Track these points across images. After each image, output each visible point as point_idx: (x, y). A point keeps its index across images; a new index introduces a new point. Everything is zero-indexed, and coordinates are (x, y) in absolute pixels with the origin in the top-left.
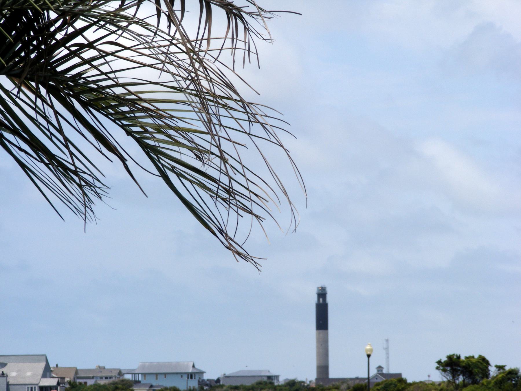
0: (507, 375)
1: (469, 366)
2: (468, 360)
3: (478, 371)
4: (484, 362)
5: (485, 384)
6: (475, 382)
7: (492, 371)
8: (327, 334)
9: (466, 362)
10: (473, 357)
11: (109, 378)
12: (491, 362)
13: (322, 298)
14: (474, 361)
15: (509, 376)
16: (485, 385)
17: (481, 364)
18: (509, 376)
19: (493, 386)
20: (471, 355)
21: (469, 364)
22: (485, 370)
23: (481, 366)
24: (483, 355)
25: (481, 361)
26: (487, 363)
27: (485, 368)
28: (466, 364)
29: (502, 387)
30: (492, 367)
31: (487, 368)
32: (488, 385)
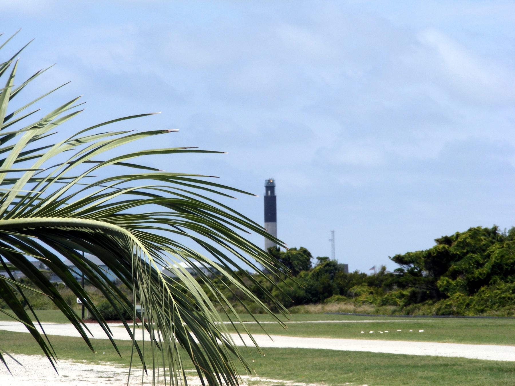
0: (324, 267)
1: (289, 258)
2: (288, 252)
3: (298, 263)
4: (305, 254)
5: (303, 276)
6: (295, 273)
7: (314, 263)
8: (276, 226)
9: (286, 254)
10: (295, 249)
11: (374, 356)
12: (312, 254)
13: (270, 190)
14: (294, 253)
15: (326, 268)
16: (303, 277)
17: (302, 256)
18: (326, 268)
19: (311, 278)
20: (294, 247)
21: (289, 256)
22: (305, 262)
23: (301, 259)
24: (305, 247)
25: (302, 253)
26: (309, 255)
27: (306, 260)
28: (285, 256)
29: (319, 279)
30: (314, 259)
31: (309, 260)
32: (305, 278)
